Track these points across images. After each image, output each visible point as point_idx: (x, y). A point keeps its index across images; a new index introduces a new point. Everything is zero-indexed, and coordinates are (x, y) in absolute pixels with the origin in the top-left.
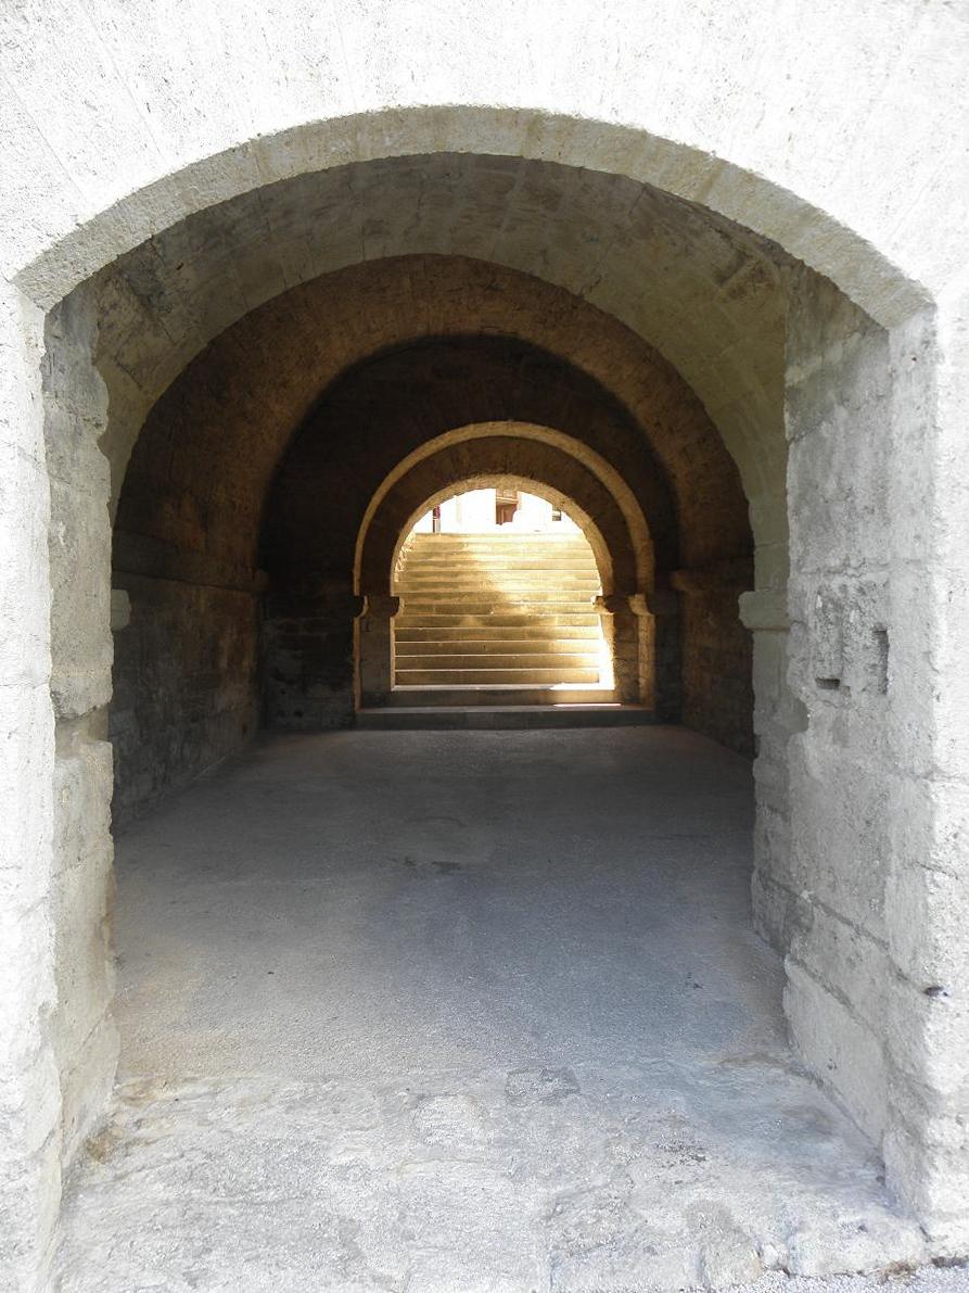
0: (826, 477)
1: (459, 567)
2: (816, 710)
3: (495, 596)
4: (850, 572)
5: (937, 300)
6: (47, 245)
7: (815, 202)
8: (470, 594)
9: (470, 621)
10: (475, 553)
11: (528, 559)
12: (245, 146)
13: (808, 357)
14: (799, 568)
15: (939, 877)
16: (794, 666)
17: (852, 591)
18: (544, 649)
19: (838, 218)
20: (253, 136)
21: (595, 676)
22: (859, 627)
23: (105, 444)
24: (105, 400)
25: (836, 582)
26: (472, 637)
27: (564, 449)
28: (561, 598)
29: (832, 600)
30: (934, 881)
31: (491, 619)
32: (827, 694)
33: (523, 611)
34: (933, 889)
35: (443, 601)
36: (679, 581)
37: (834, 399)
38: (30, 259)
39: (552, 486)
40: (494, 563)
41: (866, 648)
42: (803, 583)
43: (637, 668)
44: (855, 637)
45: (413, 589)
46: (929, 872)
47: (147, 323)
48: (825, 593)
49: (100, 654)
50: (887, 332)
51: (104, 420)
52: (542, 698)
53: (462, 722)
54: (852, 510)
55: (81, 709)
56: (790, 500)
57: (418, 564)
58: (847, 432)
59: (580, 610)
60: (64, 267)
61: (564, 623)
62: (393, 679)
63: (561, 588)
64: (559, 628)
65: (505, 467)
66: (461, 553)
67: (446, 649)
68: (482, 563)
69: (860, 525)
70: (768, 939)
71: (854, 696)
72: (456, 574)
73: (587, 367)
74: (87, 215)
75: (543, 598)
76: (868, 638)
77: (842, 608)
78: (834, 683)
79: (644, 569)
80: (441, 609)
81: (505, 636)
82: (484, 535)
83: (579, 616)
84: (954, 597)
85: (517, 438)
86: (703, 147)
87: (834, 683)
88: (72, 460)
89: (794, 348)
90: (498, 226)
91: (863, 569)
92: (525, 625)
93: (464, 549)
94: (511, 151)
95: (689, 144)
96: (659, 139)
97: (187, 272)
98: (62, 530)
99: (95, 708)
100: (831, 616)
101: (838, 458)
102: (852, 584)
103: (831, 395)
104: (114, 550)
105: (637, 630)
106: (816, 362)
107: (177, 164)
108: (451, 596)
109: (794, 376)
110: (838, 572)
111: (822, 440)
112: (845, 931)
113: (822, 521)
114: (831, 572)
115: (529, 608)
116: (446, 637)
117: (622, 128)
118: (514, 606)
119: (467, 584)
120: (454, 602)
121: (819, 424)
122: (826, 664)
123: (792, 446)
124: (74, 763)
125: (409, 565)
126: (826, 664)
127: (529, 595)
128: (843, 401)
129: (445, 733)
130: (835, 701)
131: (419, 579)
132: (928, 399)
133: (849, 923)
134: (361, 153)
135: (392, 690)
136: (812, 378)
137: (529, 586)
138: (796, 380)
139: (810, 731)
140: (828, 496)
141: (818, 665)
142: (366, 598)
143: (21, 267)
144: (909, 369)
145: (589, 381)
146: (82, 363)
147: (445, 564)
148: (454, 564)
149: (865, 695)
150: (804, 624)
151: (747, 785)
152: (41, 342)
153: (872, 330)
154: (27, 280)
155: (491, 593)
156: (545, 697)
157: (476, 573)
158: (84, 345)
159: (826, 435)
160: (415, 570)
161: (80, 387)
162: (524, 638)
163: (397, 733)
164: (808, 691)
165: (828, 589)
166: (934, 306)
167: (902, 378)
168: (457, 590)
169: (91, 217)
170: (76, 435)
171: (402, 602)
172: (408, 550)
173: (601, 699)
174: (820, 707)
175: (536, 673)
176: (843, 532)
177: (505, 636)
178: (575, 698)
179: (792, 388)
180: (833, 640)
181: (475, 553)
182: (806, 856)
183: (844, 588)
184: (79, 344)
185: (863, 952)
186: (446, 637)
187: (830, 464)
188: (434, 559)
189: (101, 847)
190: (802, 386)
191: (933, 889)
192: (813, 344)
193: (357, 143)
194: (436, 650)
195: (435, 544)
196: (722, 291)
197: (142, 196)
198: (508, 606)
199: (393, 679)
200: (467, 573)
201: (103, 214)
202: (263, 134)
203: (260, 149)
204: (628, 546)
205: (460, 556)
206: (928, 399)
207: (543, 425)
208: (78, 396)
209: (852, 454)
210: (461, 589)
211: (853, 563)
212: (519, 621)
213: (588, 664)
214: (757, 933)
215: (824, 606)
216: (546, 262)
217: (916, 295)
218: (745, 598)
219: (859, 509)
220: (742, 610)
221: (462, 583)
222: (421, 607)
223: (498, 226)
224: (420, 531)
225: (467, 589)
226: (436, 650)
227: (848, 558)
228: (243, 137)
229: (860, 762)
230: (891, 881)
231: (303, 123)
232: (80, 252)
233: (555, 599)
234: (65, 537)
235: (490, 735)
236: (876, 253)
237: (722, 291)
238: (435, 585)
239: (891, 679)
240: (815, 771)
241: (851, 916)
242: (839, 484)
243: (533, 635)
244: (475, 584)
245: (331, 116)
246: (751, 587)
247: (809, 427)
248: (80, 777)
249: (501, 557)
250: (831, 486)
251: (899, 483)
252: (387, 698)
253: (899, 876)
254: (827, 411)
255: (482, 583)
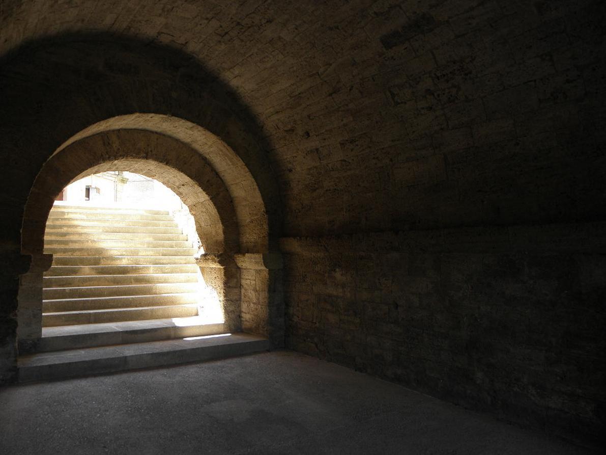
1: (65, 230)
3: (99, 251)
8: (81, 250)
9: (86, 271)
10: (77, 220)
11: (116, 225)
18: (148, 291)
21: (194, 312)
26: (91, 283)
27: (196, 146)
28: (148, 253)
31: (102, 269)
33: (124, 262)
36: (294, 246)
39: (182, 172)
40: (93, 227)
43: (239, 306)
52: (172, 334)
59: (165, 261)
61: (156, 271)
63: (145, 246)
64: (154, 275)
65: (147, 154)
66: (62, 219)
67: (72, 294)
68: (83, 227)
72: (64, 235)
73: (234, 83)
75: (135, 253)
79: (253, 234)
81: (116, 282)
82: (78, 208)
83: (168, 266)
85: (156, 133)
92: (129, 273)
93: (66, 217)
104: (157, 112)
105: (240, 278)
115: (128, 260)
116: (68, 283)
118: (118, 259)
119: (75, 242)
120: (67, 256)
127: (126, 251)
137: (124, 245)
145: (232, 95)
148: (61, 227)
155: (97, 249)
156: (172, 334)
157: (80, 234)
162: (131, 283)
168: (67, 247)
173: (215, 331)
175: (152, 311)
177: (116, 282)
178: (197, 331)
181: (77, 220)
186: (68, 283)
194: (63, 295)
198: (112, 258)
200: (73, 234)
204: (234, 218)
205: (67, 221)
207: (194, 122)
210: (72, 246)
212: (124, 270)
213: (197, 303)
221: (73, 242)
225: (76, 246)
226: (63, 295)
233: (144, 254)
243: (138, 280)
244: (82, 242)
249: (96, 223)
252: (41, 346)
255: (88, 241)
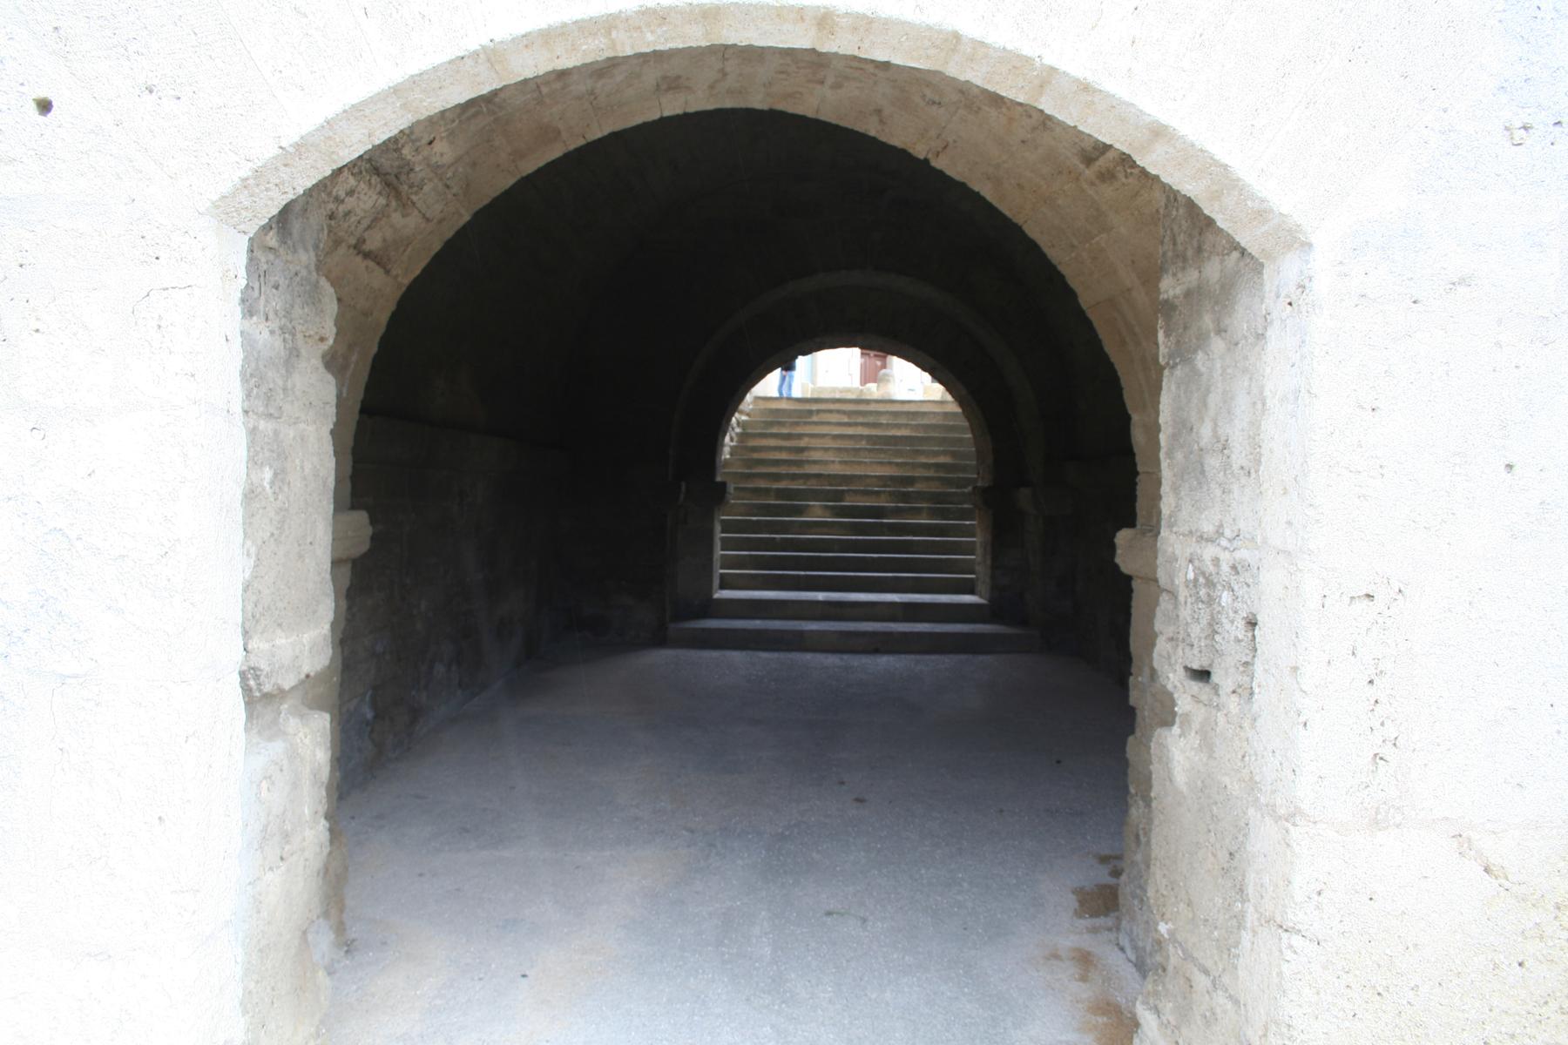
0: (1202, 420)
2: (1183, 704)
4: (1224, 543)
5: (1313, 240)
6: (245, 171)
7: (1164, 119)
12: (476, 54)
13: (1184, 269)
14: (1171, 526)
15: (1296, 941)
16: (1161, 646)
17: (1225, 568)
19: (1191, 138)
20: (486, 42)
22: (1231, 614)
23: (333, 362)
24: (331, 307)
25: (1209, 552)
29: (1203, 574)
30: (1291, 947)
32: (1195, 686)
34: (1289, 955)
35: (782, 485)
37: (1211, 326)
38: (226, 187)
41: (1238, 641)
42: (1172, 542)
44: (1227, 626)
45: (749, 467)
46: (1285, 935)
47: (394, 203)
48: (1197, 563)
49: (315, 612)
50: (1262, 265)
51: (330, 331)
53: (798, 642)
54: (1226, 466)
55: (288, 682)
56: (1163, 438)
57: (754, 436)
58: (1224, 369)
60: (267, 190)
62: (716, 582)
69: (1235, 487)
70: (1133, 958)
71: (1223, 698)
72: (801, 450)
74: (291, 137)
76: (1238, 629)
77: (1214, 585)
78: (1203, 675)
80: (781, 494)
84: (1327, 602)
86: (1027, 51)
87: (1203, 675)
88: (285, 390)
89: (1170, 254)
90: (822, 83)
91: (1236, 543)
94: (804, 43)
95: (1009, 47)
96: (973, 41)
97: (439, 146)
98: (268, 474)
99: (308, 676)
100: (1203, 592)
101: (1214, 399)
102: (1225, 557)
103: (1207, 321)
106: (1191, 277)
107: (397, 76)
108: (794, 477)
109: (1170, 287)
110: (1210, 540)
111: (1196, 373)
112: (1201, 982)
113: (1196, 471)
114: (1202, 539)
117: (929, 28)
121: (1195, 351)
122: (1196, 651)
123: (1166, 372)
124: (278, 747)
125: (743, 436)
126: (1196, 651)
128: (1220, 331)
129: (775, 655)
130: (1204, 697)
131: (756, 456)
132: (1303, 357)
133: (1206, 972)
134: (619, 48)
135: (716, 596)
136: (1188, 294)
138: (1171, 293)
139: (1176, 730)
140: (1202, 444)
141: (1187, 649)
142: (683, 485)
143: (215, 197)
144: (1284, 315)
146: (304, 273)
147: (789, 437)
149: (1234, 698)
150: (1173, 595)
151: (1123, 764)
152: (243, 273)
153: (1248, 263)
154: (225, 209)
158: (306, 250)
159: (1203, 369)
160: (752, 443)
161: (298, 301)
163: (715, 654)
164: (1174, 678)
165: (1200, 559)
166: (1310, 245)
167: (1277, 324)
169: (296, 139)
170: (294, 353)
171: (731, 488)
172: (744, 418)
174: (1186, 695)
176: (1218, 492)
179: (1166, 301)
180: (1204, 622)
182: (1164, 882)
183: (1216, 561)
184: (301, 251)
185: (1218, 1010)
187: (1205, 404)
188: (775, 430)
189: (313, 834)
190: (1177, 302)
191: (1289, 955)
192: (1190, 253)
193: (613, 41)
195: (778, 411)
196: (1089, 173)
197: (356, 112)
199: (716, 582)
201: (310, 134)
202: (497, 40)
203: (491, 55)
206: (1303, 357)
208: (297, 311)
209: (1228, 398)
211: (1228, 533)
214: (1122, 949)
215: (1196, 580)
216: (881, 121)
217: (1290, 231)
218: (1123, 537)
219: (1235, 467)
220: (1119, 552)
222: (757, 492)
223: (822, 83)
224: (761, 394)
227: (1221, 526)
228: (473, 44)
229: (1226, 780)
230: (1246, 937)
231: (544, 26)
232: (285, 174)
234: (272, 483)
235: (832, 660)
236: (1238, 180)
237: (1089, 173)
238: (777, 462)
239: (1256, 690)
240: (1180, 778)
241: (1209, 964)
242: (1215, 430)
245: (578, 17)
246: (1132, 525)
247: (1184, 354)
248: (285, 762)
250: (1206, 432)
251: (1271, 451)
253: (1255, 933)
254: (1202, 339)
